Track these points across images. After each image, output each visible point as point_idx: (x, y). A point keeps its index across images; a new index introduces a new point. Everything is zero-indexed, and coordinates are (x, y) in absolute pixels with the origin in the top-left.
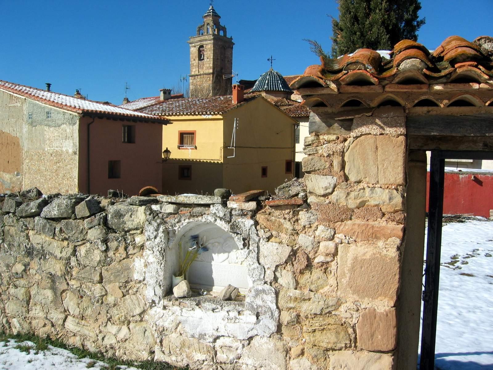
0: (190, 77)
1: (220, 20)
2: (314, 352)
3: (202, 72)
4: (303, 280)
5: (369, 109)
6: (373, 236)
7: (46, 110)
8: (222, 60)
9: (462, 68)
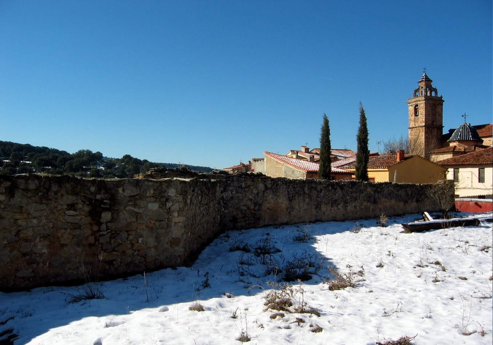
3: (417, 125)
7: (292, 170)
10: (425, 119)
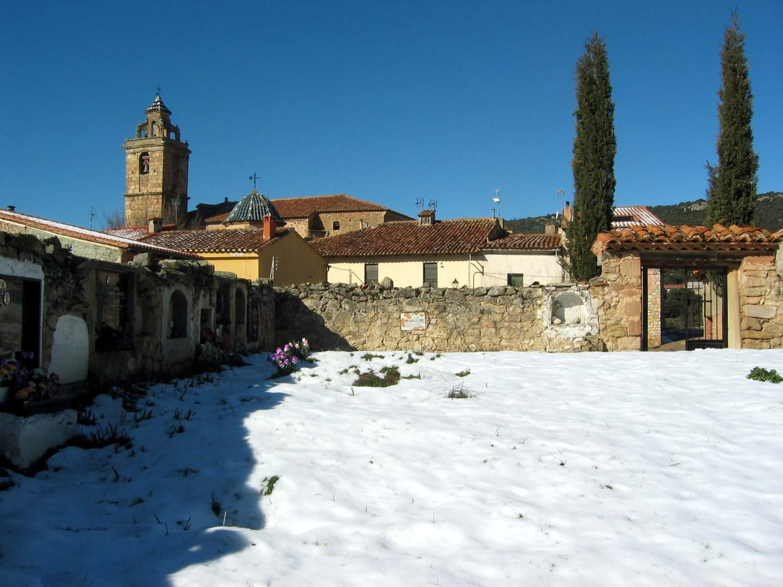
0: (126, 198)
1: (171, 117)
2: (613, 339)
4: (607, 313)
5: (628, 251)
6: (632, 294)
8: (175, 174)
9: (660, 238)
10: (164, 180)
